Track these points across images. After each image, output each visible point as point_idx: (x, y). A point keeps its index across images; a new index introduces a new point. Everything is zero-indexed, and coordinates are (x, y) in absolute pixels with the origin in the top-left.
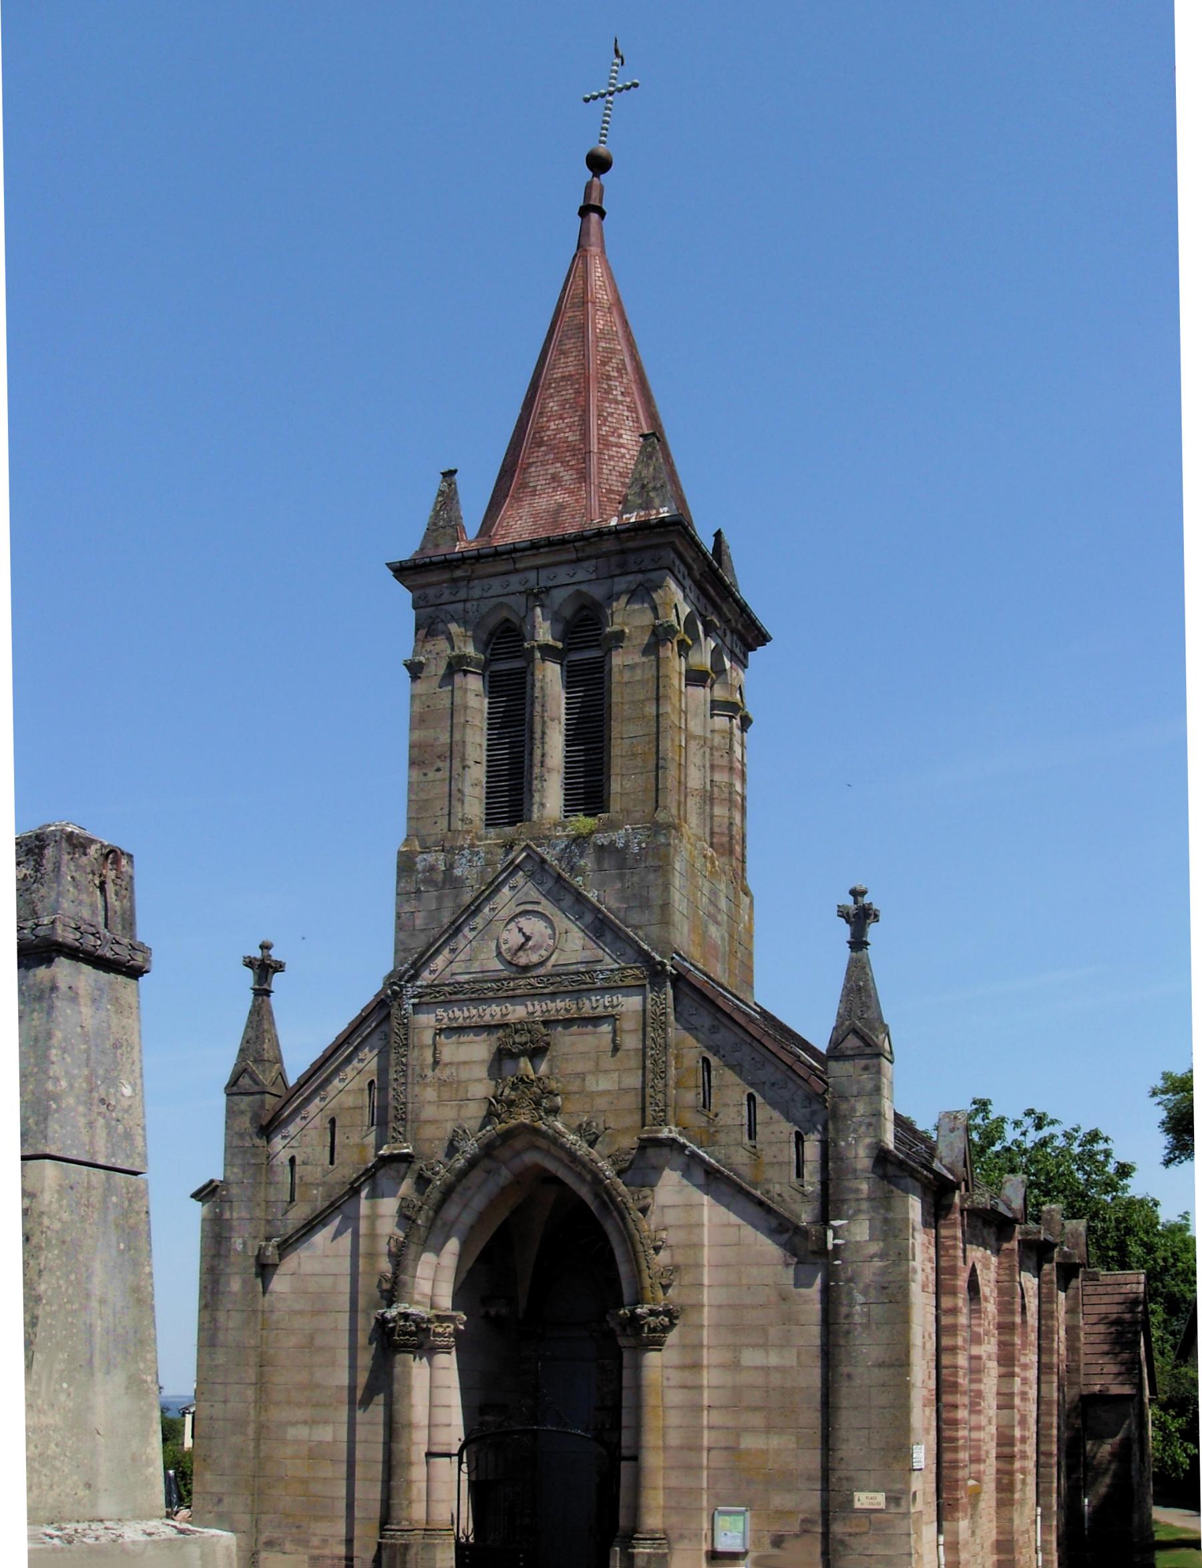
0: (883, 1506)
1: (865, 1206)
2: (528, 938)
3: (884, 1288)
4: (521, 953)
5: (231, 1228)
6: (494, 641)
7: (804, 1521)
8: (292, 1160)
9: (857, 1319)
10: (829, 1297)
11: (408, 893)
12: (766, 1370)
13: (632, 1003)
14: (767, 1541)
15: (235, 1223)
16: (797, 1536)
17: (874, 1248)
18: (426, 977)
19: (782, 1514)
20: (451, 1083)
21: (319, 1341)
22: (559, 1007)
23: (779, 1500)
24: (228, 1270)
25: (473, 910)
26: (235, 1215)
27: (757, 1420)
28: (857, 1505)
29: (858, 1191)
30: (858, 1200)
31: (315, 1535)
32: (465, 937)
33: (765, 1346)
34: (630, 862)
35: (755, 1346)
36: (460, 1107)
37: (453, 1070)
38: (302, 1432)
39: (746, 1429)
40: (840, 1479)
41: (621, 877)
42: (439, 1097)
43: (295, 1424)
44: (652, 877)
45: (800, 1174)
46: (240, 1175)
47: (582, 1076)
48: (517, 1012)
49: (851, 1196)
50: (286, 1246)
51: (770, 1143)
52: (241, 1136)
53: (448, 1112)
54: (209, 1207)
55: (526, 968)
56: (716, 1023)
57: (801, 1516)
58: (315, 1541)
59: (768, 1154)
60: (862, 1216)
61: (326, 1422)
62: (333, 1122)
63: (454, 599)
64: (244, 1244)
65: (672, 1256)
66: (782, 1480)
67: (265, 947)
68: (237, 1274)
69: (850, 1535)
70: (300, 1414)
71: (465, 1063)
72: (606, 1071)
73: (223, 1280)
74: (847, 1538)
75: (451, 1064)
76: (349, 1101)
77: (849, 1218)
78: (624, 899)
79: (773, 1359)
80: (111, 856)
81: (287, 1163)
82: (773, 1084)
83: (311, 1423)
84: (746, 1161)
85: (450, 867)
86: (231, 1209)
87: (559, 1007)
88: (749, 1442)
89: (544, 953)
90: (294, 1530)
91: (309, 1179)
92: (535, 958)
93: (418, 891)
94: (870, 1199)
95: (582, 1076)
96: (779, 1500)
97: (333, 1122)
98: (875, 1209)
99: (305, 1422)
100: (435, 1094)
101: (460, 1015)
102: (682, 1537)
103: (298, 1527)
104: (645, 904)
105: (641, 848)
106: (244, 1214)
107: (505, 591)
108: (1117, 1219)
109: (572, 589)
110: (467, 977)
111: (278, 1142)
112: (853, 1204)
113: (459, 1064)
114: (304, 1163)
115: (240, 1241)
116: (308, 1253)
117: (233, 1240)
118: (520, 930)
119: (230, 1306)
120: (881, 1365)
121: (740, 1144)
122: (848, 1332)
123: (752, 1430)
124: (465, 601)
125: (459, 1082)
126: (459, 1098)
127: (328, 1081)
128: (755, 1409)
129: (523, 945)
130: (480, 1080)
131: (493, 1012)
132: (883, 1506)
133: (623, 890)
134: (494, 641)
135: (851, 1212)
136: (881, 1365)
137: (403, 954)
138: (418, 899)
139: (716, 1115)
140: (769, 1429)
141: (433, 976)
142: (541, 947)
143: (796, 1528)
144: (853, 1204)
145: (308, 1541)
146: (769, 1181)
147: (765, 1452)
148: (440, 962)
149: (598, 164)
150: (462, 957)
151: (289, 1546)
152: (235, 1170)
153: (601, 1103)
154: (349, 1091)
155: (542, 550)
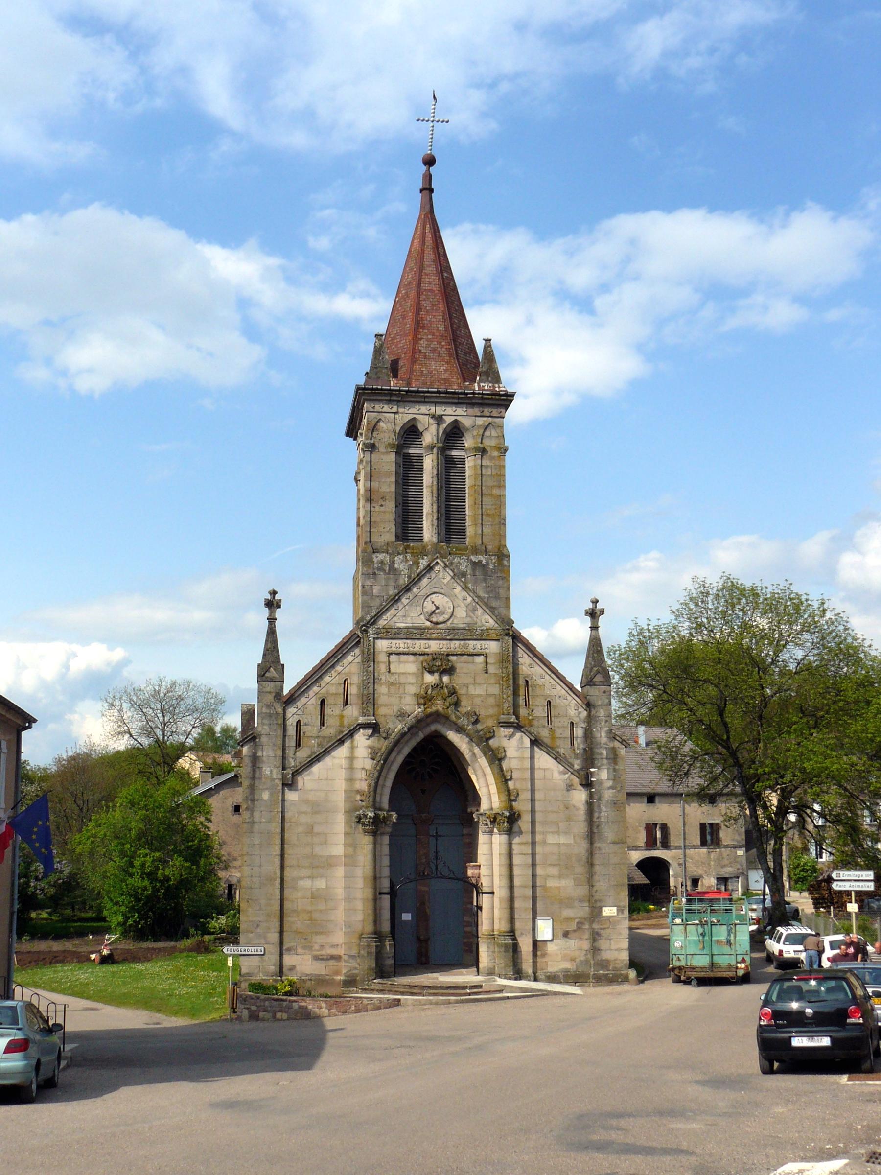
0: (615, 914)
1: (605, 761)
2: (437, 608)
3: (615, 804)
4: (433, 615)
5: (263, 762)
6: (405, 436)
7: (578, 923)
8: (298, 722)
9: (603, 819)
10: (591, 796)
11: (369, 574)
12: (559, 844)
13: (493, 647)
14: (560, 934)
15: (264, 759)
16: (574, 931)
17: (610, 783)
18: (382, 623)
19: (568, 919)
20: (395, 684)
21: (317, 829)
22: (455, 645)
23: (567, 913)
24: (261, 787)
25: (407, 589)
26: (265, 754)
27: (554, 871)
28: (604, 914)
29: (602, 754)
30: (602, 758)
31: (316, 943)
32: (402, 603)
33: (558, 833)
34: (489, 573)
35: (553, 833)
36: (401, 697)
37: (397, 677)
38: (306, 883)
39: (549, 876)
40: (596, 901)
41: (485, 580)
42: (389, 691)
43: (302, 878)
44: (500, 582)
45: (572, 744)
46: (268, 730)
47: (467, 686)
48: (434, 646)
49: (599, 757)
50: (297, 773)
51: (558, 727)
52: (268, 706)
53: (394, 700)
54: (248, 748)
55: (437, 623)
56: (532, 662)
57: (577, 921)
58: (316, 947)
59: (558, 733)
60: (604, 767)
61: (322, 877)
62: (323, 702)
63: (390, 411)
64: (271, 771)
65: (515, 785)
66: (567, 902)
67: (274, 593)
68: (267, 789)
69: (601, 929)
70: (304, 872)
71: (403, 673)
72: (479, 684)
73: (256, 791)
74: (599, 931)
75: (396, 673)
76: (333, 690)
77: (599, 768)
78: (488, 593)
79: (563, 840)
80: (434, 620)
81: (295, 724)
82: (560, 697)
83: (311, 877)
84: (547, 735)
85: (393, 562)
86: (262, 750)
87: (455, 645)
88: (551, 883)
89: (447, 617)
90: (303, 941)
91: (307, 734)
92: (441, 619)
93: (374, 574)
94: (607, 758)
95: (467, 686)
96: (567, 913)
97: (323, 702)
98: (609, 764)
99: (309, 877)
100: (387, 690)
101: (401, 645)
102: (522, 934)
103: (305, 939)
104: (497, 597)
105: (495, 566)
106: (271, 754)
107: (418, 412)
108: (129, 717)
109: (453, 418)
110: (411, 625)
111: (291, 711)
112: (600, 760)
113: (400, 673)
114: (306, 724)
115: (268, 769)
116: (309, 778)
117: (264, 768)
118: (433, 602)
119: (262, 809)
120: (614, 843)
121: (544, 727)
122: (598, 827)
123: (553, 877)
124: (395, 413)
125: (400, 684)
126: (401, 692)
127: (321, 677)
128: (553, 865)
129: (435, 611)
130: (412, 684)
131: (419, 645)
132: (615, 914)
133: (487, 587)
134: (405, 436)
135: (599, 765)
136: (614, 843)
137: (366, 609)
138: (375, 579)
139: (532, 711)
140: (560, 877)
141: (386, 622)
142: (444, 613)
143: (574, 927)
144: (600, 760)
145: (312, 947)
146: (558, 747)
147: (558, 888)
148: (388, 616)
149: (430, 161)
150: (401, 614)
151: (300, 950)
152: (265, 727)
153: (477, 701)
154: (332, 684)
155: (442, 395)
